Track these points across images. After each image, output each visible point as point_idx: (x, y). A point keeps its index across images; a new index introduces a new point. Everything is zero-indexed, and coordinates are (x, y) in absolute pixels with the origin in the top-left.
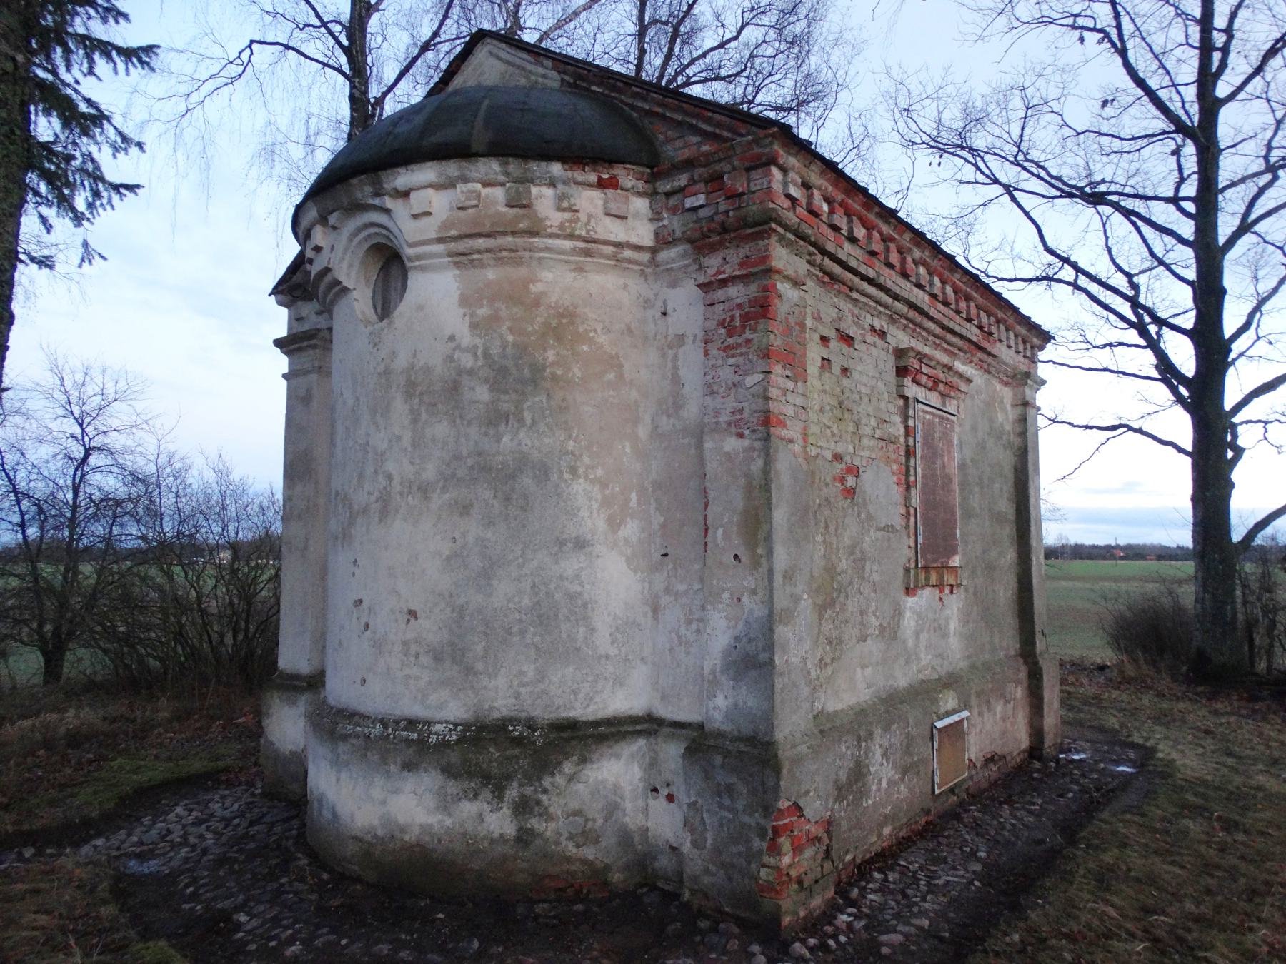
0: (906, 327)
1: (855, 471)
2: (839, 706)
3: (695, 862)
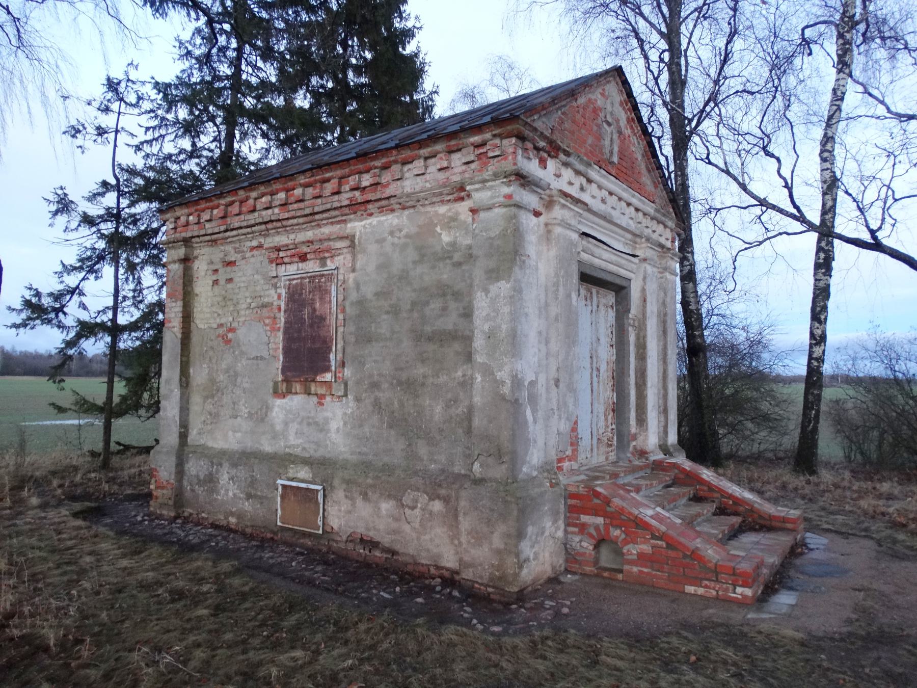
0: (278, 233)
1: (232, 330)
2: (215, 446)
3: (805, 638)
